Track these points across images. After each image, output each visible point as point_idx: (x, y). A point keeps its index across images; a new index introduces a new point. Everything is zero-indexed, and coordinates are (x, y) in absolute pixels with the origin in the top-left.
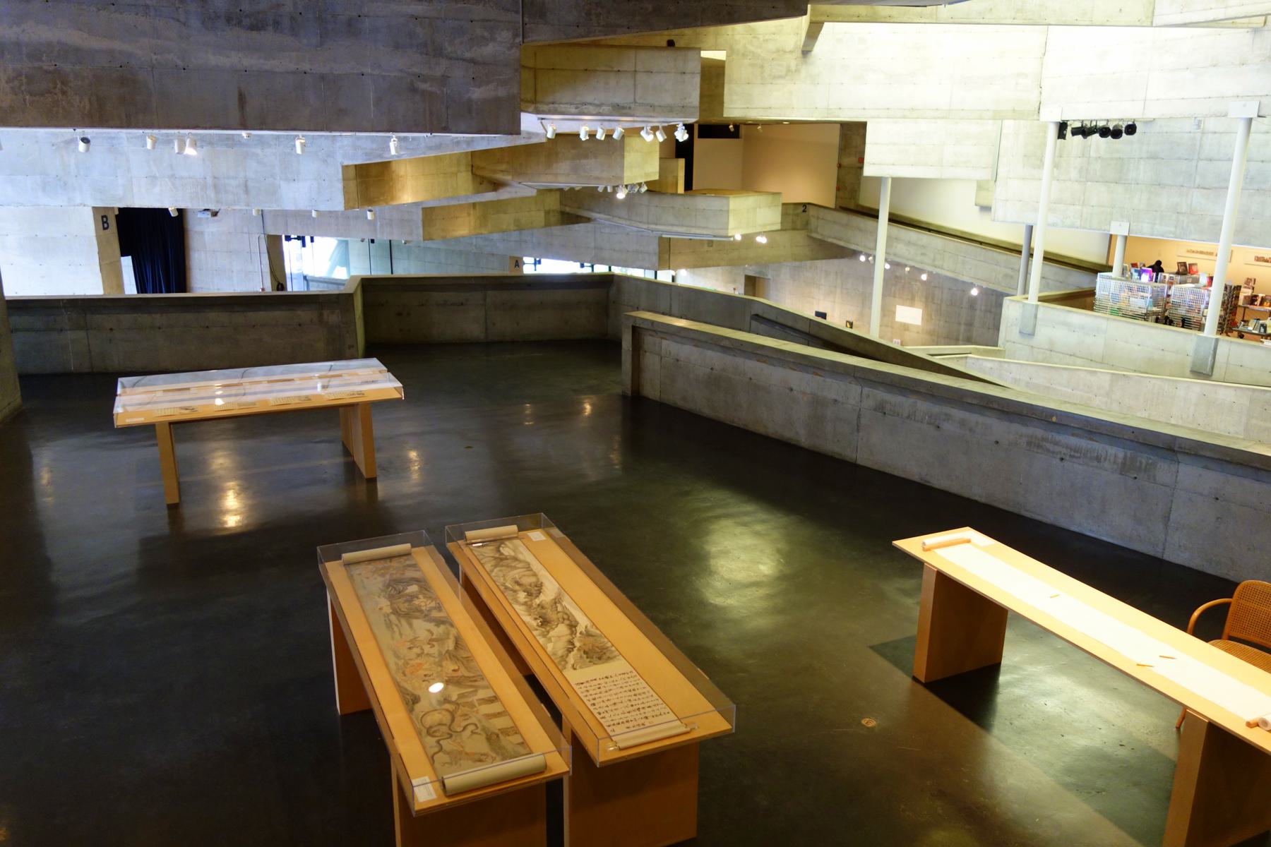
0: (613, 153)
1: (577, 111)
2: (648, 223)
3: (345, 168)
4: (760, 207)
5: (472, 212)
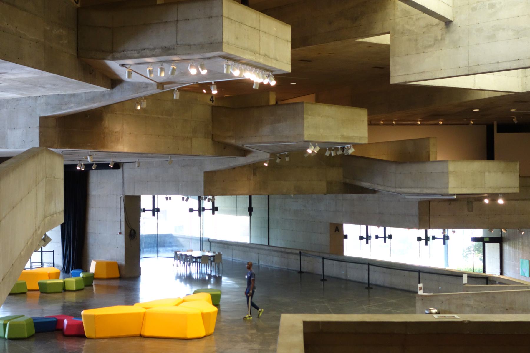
1: (139, 55)
2: (396, 188)
3: (43, 120)
4: (489, 172)
5: (252, 178)
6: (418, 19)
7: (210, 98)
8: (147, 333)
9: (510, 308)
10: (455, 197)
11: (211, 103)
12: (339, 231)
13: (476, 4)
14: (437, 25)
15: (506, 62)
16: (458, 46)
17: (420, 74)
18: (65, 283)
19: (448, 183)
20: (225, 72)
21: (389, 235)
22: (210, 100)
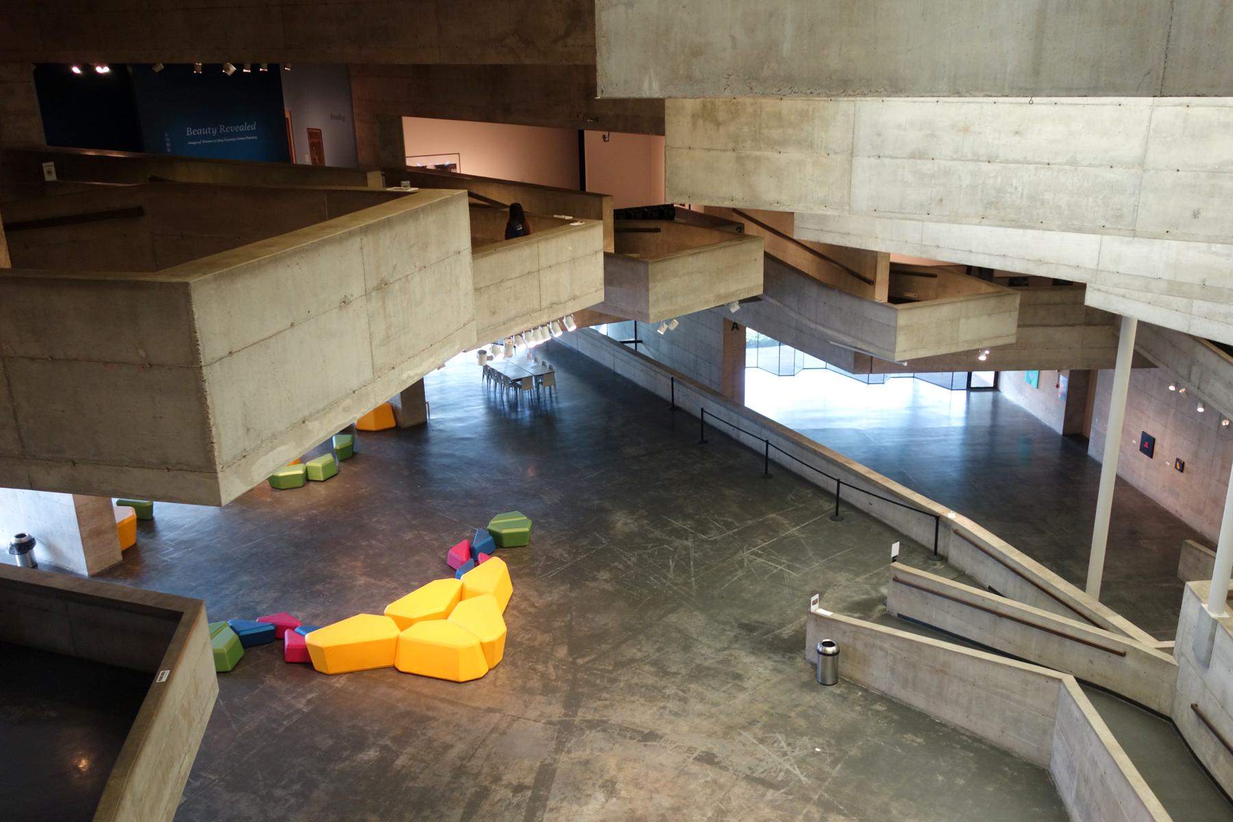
0: (638, 282)
2: (816, 323)
9: (942, 671)
12: (738, 329)
15: (983, 253)
18: (308, 469)
19: (894, 344)
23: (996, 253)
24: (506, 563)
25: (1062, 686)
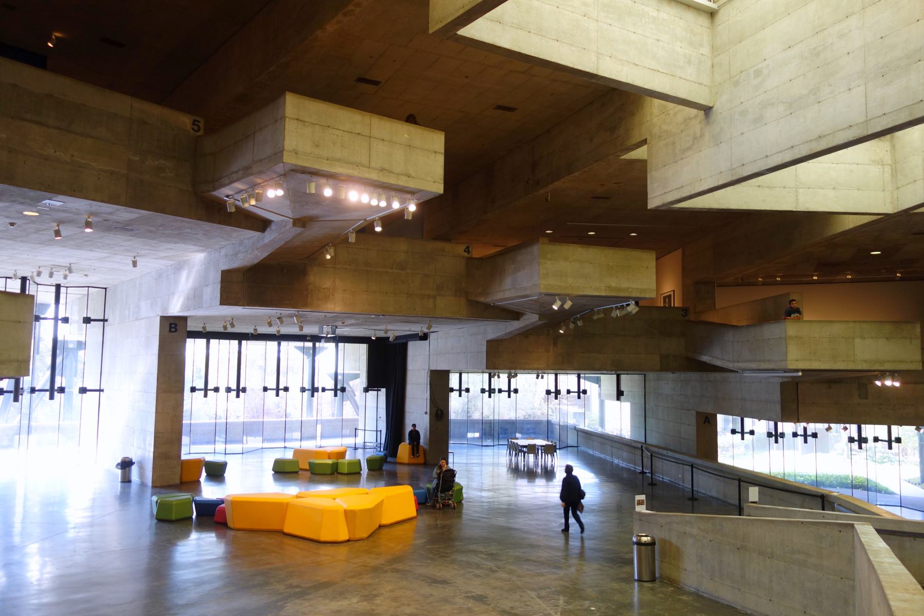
2: (734, 362)
4: (863, 338)
5: (551, 349)
6: (675, 114)
7: (464, 248)
8: (286, 530)
10: (800, 374)
11: (466, 254)
12: (709, 423)
13: (739, 75)
14: (696, 117)
16: (719, 142)
17: (678, 190)
20: (308, 192)
21: (896, 438)
22: (465, 251)
23: (786, 148)
24: (411, 486)
25: (855, 534)
